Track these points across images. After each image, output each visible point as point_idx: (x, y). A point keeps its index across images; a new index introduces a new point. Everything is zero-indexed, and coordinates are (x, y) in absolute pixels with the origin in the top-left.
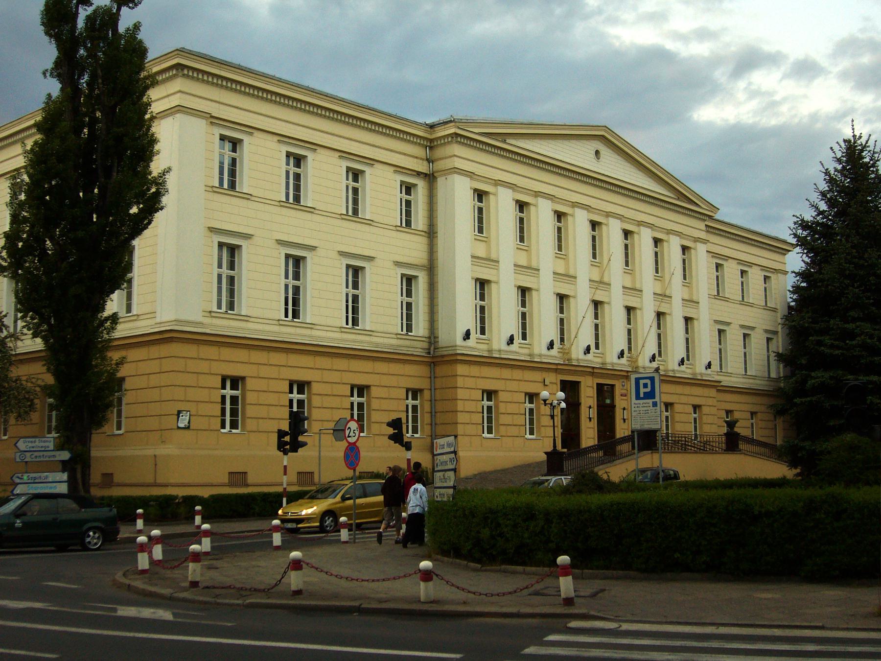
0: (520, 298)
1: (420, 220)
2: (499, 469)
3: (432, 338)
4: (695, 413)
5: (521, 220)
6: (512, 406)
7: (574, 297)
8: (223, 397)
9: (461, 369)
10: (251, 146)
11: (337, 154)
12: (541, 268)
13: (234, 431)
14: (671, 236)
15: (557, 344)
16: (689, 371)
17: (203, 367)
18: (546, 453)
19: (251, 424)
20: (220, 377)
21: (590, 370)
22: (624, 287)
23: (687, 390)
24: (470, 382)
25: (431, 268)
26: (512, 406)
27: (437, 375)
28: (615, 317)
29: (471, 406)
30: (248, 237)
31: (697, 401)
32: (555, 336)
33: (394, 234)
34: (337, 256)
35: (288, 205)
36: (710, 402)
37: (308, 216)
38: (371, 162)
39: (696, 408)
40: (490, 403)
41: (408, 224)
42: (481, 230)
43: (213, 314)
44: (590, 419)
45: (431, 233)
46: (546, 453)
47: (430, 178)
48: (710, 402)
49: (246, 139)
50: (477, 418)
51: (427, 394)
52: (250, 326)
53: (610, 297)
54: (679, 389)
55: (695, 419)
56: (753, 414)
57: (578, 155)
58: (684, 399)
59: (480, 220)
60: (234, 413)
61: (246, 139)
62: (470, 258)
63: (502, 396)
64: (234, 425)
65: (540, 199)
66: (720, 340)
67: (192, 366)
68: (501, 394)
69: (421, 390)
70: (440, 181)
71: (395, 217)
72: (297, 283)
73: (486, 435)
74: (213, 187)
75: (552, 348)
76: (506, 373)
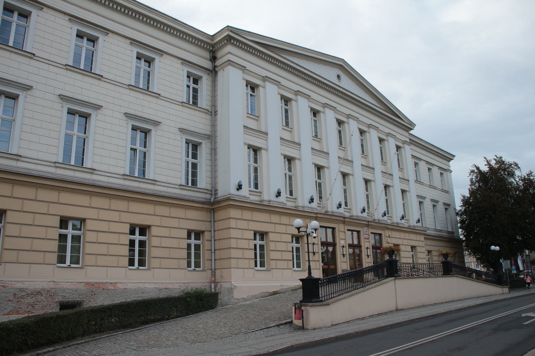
0: (317, 173)
1: (204, 100)
2: (175, 294)
3: (214, 191)
4: (412, 251)
5: (286, 111)
6: (280, 244)
7: (328, 168)
8: (189, 246)
9: (234, 213)
10: (160, 62)
11: (67, 18)
12: (301, 143)
13: (140, 268)
14: (267, 83)
15: (366, 211)
16: (406, 224)
17: (42, 208)
18: (301, 280)
19: (155, 263)
20: (186, 231)
21: (342, 219)
22: (312, 149)
23: (407, 236)
24: (242, 224)
25: (212, 137)
26: (280, 244)
27: (215, 220)
28: (332, 177)
29: (243, 244)
30: (157, 123)
31: (414, 243)
32: (364, 204)
33: (180, 108)
34: (124, 118)
35: (189, 106)
36: (421, 244)
37: (154, 100)
38: (106, 31)
39: (413, 248)
40: (298, 245)
41: (195, 103)
42: (287, 124)
43: (57, 165)
44: (368, 256)
45: (213, 112)
46: (301, 280)
47: (213, 72)
48: (421, 244)
49: (35, 12)
50: (289, 256)
51: (207, 235)
52: (94, 177)
53: (353, 170)
54: (402, 235)
55: (413, 255)
56: (429, 252)
57: (329, 74)
58: (405, 242)
59: (287, 117)
60: (142, 253)
61: (35, 12)
62: (398, 179)
63: (272, 237)
64: (75, 260)
65: (326, 109)
66: (403, 198)
67: (29, 206)
68: (271, 235)
69: (203, 232)
70: (220, 74)
71: (182, 95)
72: (194, 161)
73: (296, 269)
74: (182, 102)
75: (340, 207)
76: (275, 218)
